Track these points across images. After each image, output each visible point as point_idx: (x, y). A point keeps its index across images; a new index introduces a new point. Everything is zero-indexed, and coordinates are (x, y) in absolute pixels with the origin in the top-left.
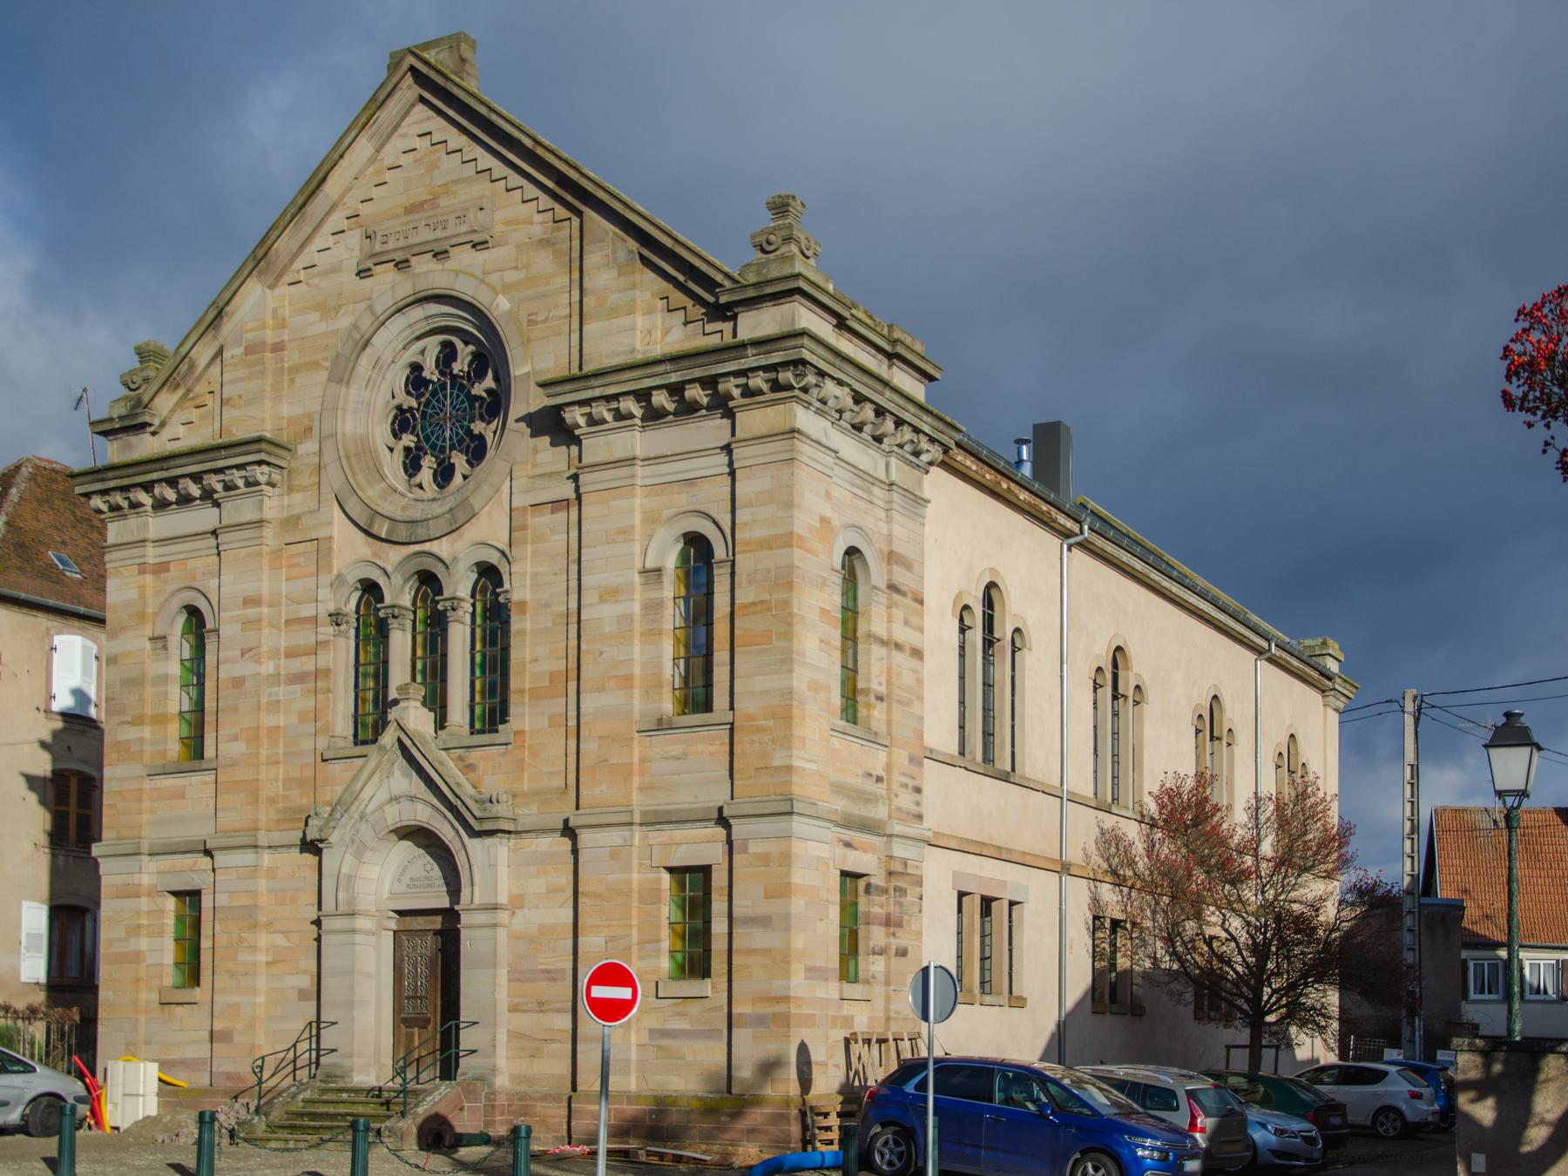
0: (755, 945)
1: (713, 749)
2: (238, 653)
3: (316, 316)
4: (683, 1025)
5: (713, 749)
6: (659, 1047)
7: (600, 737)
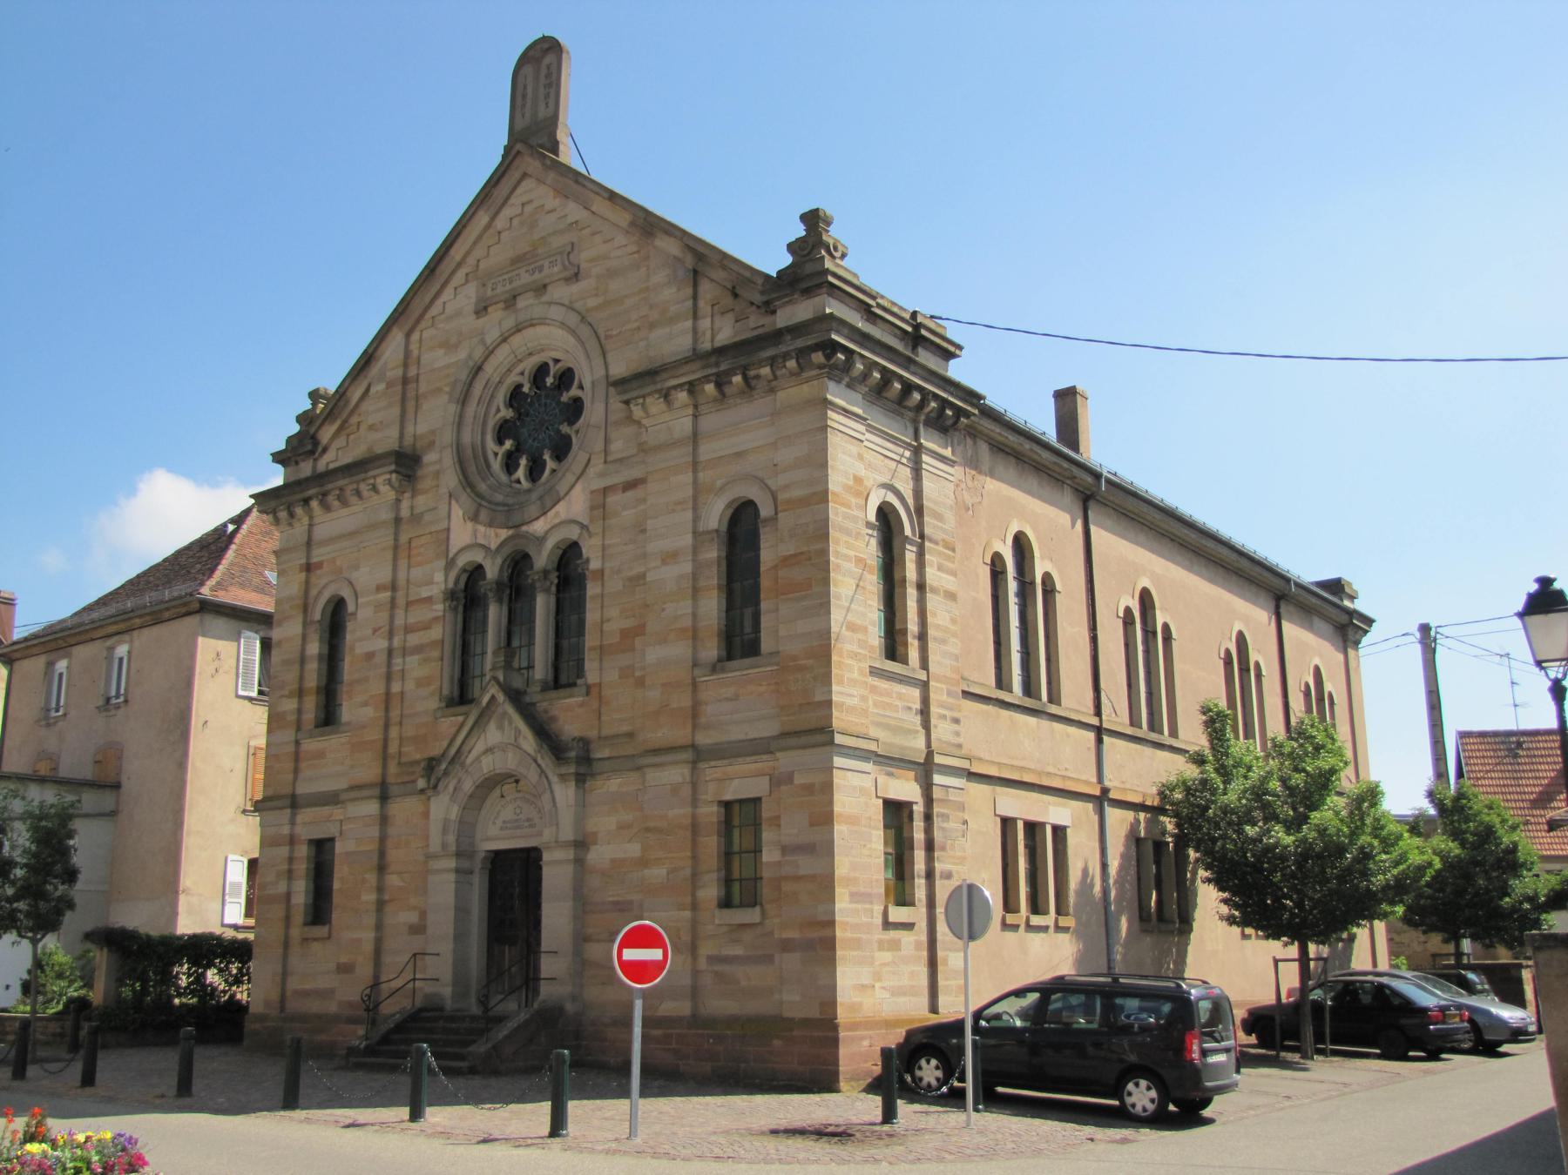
0: (802, 872)
1: (762, 689)
2: (370, 631)
3: (441, 352)
4: (738, 951)
5: (762, 689)
6: (716, 973)
7: (663, 685)
